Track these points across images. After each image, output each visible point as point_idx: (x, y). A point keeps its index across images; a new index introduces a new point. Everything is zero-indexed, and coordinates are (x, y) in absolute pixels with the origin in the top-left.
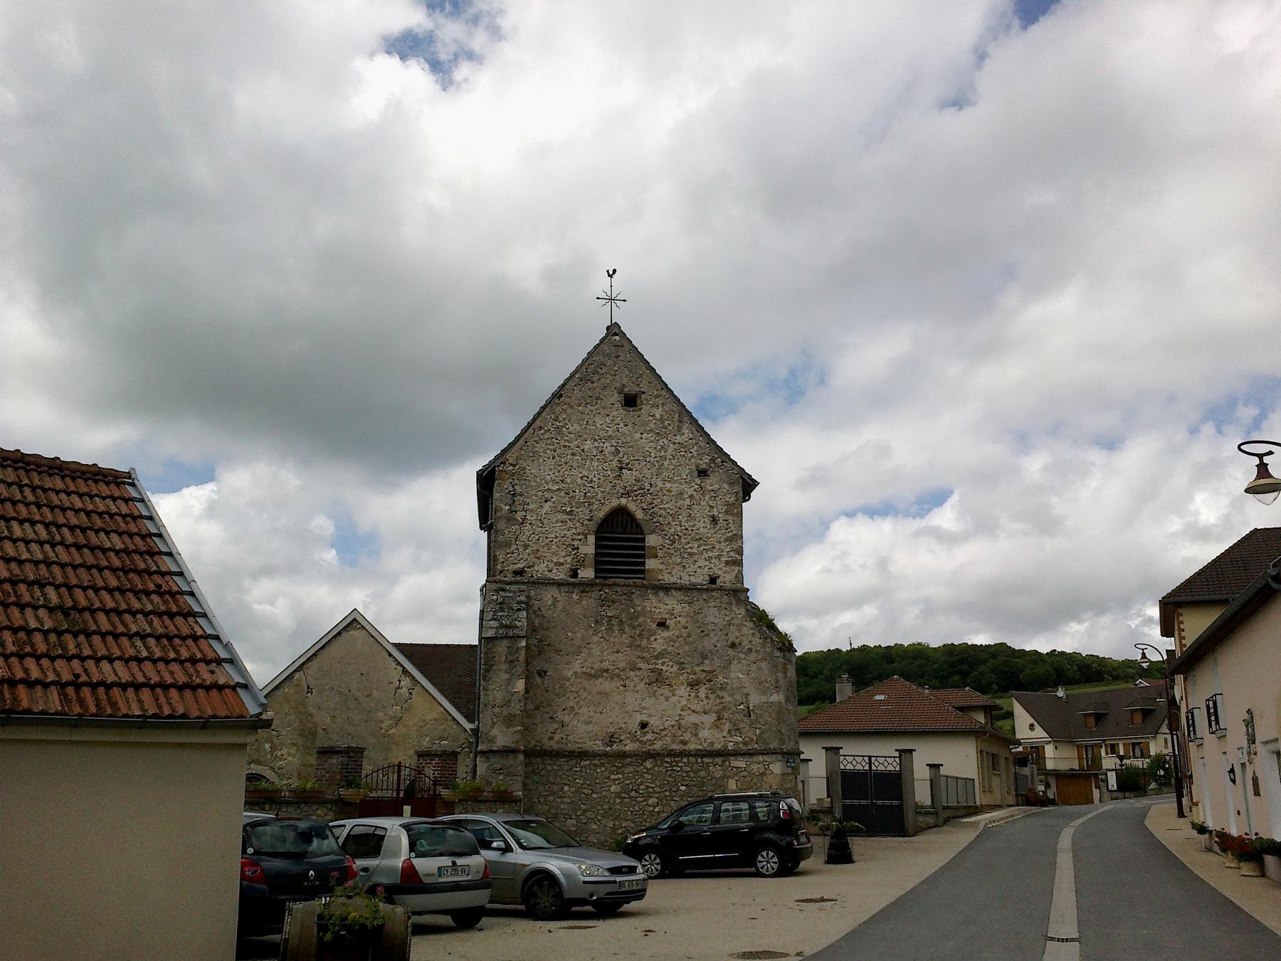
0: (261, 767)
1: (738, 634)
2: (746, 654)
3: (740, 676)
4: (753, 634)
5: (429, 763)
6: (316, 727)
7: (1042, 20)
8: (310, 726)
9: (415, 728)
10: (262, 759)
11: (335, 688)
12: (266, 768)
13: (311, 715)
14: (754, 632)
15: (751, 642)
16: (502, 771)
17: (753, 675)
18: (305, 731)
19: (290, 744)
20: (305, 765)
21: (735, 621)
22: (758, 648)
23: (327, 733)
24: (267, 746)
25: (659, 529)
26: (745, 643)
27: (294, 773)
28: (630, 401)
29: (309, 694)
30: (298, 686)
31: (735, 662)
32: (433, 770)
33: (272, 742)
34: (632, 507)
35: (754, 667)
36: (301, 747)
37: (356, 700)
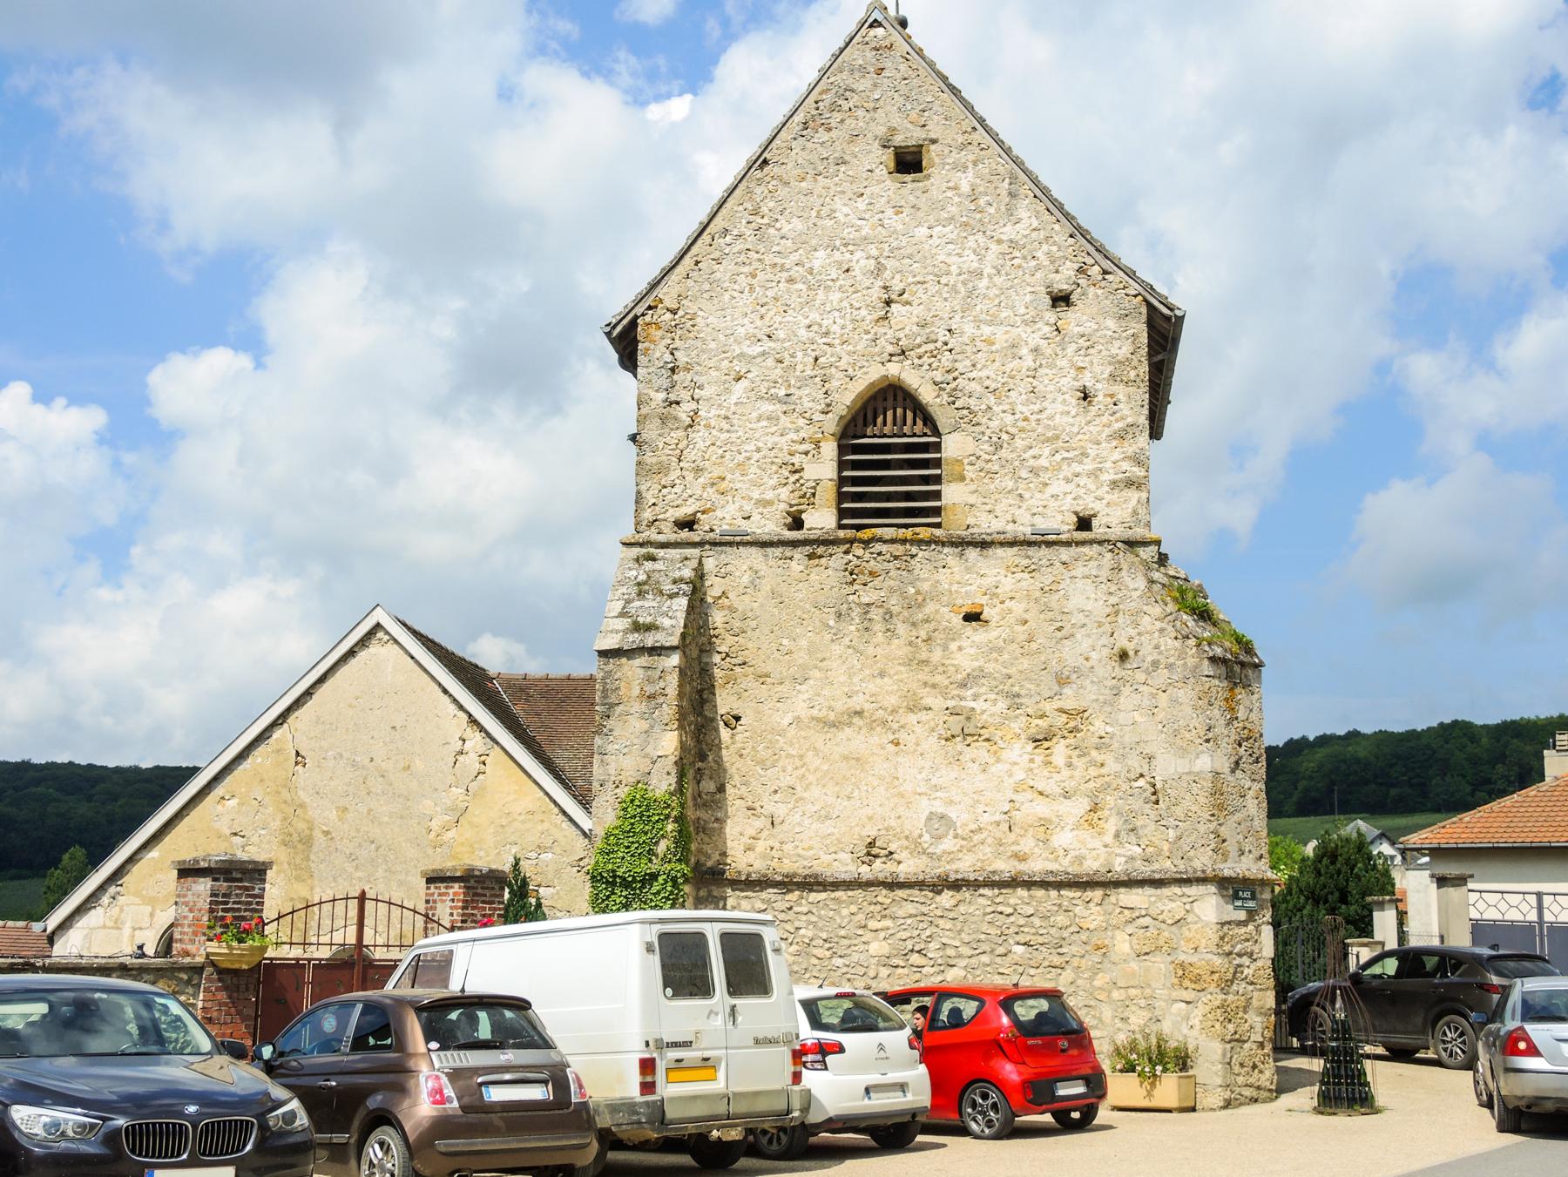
4: (1162, 630)
6: (311, 829)
8: (301, 825)
13: (302, 806)
22: (1171, 660)
32: (451, 908)
35: (1163, 699)
37: (383, 776)
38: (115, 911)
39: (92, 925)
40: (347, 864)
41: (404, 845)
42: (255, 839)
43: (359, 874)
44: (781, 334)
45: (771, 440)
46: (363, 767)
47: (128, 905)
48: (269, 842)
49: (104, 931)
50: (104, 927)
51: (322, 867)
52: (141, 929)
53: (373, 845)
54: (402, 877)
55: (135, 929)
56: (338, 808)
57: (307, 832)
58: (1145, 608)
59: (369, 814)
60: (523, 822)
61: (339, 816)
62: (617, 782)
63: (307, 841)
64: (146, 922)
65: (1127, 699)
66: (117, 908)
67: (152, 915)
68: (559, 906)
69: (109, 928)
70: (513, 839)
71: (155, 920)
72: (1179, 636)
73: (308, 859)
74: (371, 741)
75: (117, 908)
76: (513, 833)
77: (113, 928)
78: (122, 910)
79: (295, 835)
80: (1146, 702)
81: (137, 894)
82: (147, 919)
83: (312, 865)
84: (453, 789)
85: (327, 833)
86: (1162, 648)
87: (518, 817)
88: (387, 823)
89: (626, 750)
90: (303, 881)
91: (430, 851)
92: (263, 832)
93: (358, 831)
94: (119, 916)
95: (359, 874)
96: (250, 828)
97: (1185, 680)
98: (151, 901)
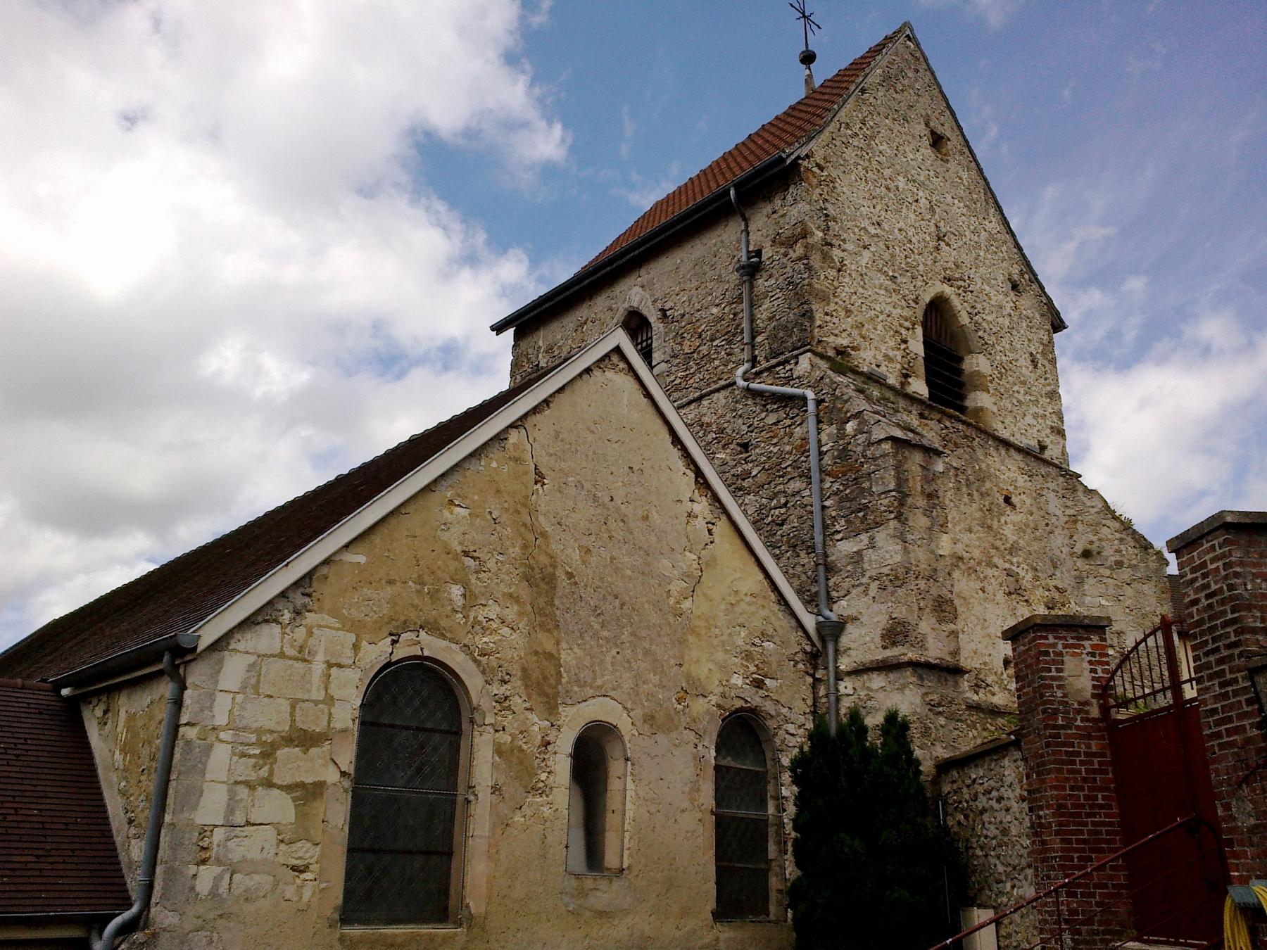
0: (445, 643)
1: (1095, 538)
2: (1110, 568)
3: (1104, 602)
4: (1121, 540)
5: (1073, 646)
6: (555, 567)
7: (88, 734)
8: (544, 560)
9: (723, 607)
10: (444, 623)
11: (587, 486)
12: (453, 646)
13: (544, 535)
14: (1123, 536)
15: (1118, 551)
16: (941, 709)
17: (1129, 602)
18: (533, 569)
19: (504, 594)
20: (536, 653)
21: (1087, 518)
22: (1134, 562)
23: (576, 583)
24: (456, 591)
25: (985, 349)
26: (1108, 551)
27: (516, 670)
28: (937, 141)
29: (539, 485)
30: (517, 460)
31: (1091, 581)
32: (1090, 662)
33: (466, 585)
34: (956, 302)
35: (1129, 591)
36: (529, 608)
37: (623, 521)
38: (300, 633)
39: (263, 649)
40: (592, 619)
41: (646, 606)
42: (491, 564)
43: (605, 633)
44: (886, 226)
45: (889, 308)
46: (604, 505)
47: (319, 626)
48: (508, 573)
49: (280, 663)
50: (282, 655)
51: (568, 616)
52: (340, 666)
53: (617, 601)
54: (647, 645)
55: (330, 665)
56: (580, 547)
57: (550, 569)
58: (1104, 522)
59: (611, 562)
60: (749, 604)
61: (581, 557)
62: (917, 573)
63: (550, 580)
64: (347, 656)
65: (1090, 585)
66: (303, 630)
67: (356, 647)
68: (782, 701)
69: (290, 658)
70: (741, 620)
71: (360, 655)
72: (1137, 546)
73: (551, 603)
74: (611, 478)
75: (303, 630)
76: (741, 614)
77: (296, 659)
78: (310, 633)
79: (537, 570)
80: (1111, 591)
81: (334, 613)
82: (349, 652)
83: (558, 613)
84: (687, 553)
85: (570, 576)
86: (1124, 552)
87: (744, 598)
88: (630, 578)
89: (919, 543)
90: (549, 630)
91: (671, 619)
92: (501, 558)
93: (601, 579)
94: (306, 641)
95: (605, 633)
96: (486, 550)
97: (1149, 579)
98: (354, 626)
